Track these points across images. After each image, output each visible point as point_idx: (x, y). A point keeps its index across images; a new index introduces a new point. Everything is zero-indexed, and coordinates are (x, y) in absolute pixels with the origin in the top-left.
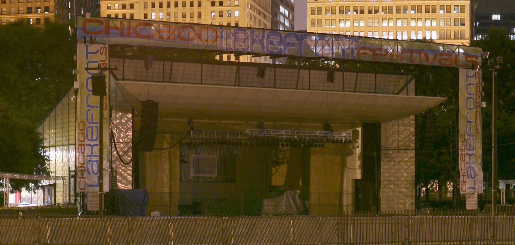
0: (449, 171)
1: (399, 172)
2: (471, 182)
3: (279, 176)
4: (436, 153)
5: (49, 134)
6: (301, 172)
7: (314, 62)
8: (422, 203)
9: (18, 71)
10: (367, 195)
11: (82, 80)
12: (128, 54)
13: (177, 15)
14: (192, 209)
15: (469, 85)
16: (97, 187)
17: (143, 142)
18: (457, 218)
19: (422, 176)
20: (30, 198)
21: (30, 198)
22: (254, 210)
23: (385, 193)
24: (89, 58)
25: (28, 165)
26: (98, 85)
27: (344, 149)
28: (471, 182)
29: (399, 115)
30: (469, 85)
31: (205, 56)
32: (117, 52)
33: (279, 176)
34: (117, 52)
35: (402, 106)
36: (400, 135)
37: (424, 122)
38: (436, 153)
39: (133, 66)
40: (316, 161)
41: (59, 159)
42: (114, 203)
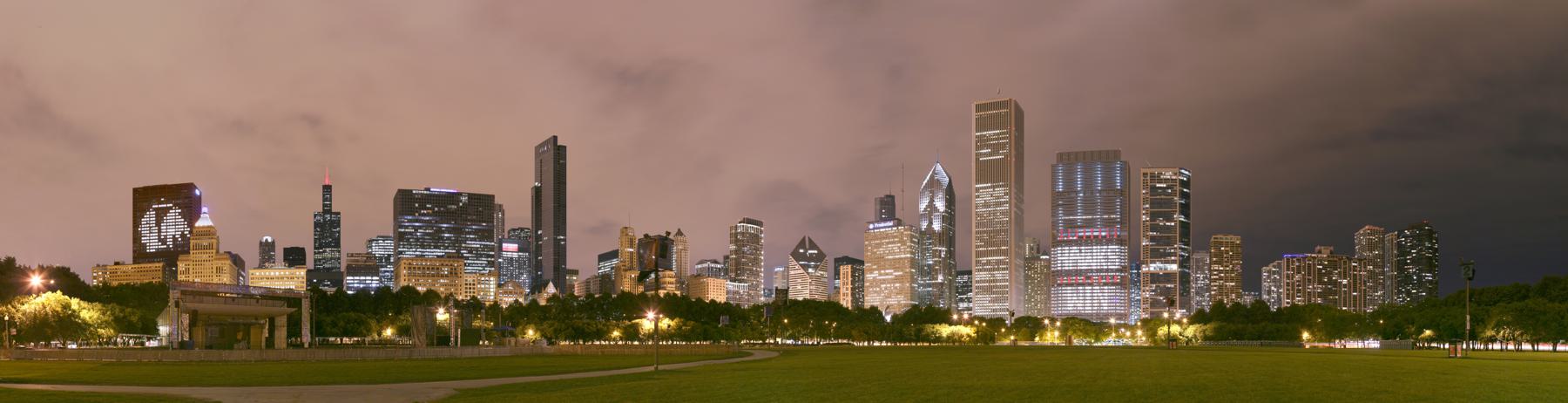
0: (299, 334)
1: (281, 334)
2: (306, 338)
3: (240, 336)
4: (294, 327)
5: (160, 321)
6: (247, 334)
7: (252, 296)
8: (289, 345)
9: (543, 303)
10: (270, 342)
11: (171, 303)
12: (1374, 344)
13: (204, 280)
14: (210, 347)
15: (306, 304)
16: (177, 339)
17: (192, 324)
18: (301, 351)
19: (289, 336)
20: (153, 344)
21: (153, 344)
22: (231, 348)
23: (277, 342)
24: (174, 295)
25: (152, 331)
26: (177, 304)
27: (262, 326)
28: (306, 338)
29: (281, 315)
30: (306, 304)
31: (214, 294)
32: (183, 293)
33: (240, 336)
34: (183, 293)
35: (282, 312)
36: (282, 322)
37: (290, 317)
38: (294, 327)
39: (189, 298)
40: (253, 331)
41: (163, 330)
42: (182, 345)
